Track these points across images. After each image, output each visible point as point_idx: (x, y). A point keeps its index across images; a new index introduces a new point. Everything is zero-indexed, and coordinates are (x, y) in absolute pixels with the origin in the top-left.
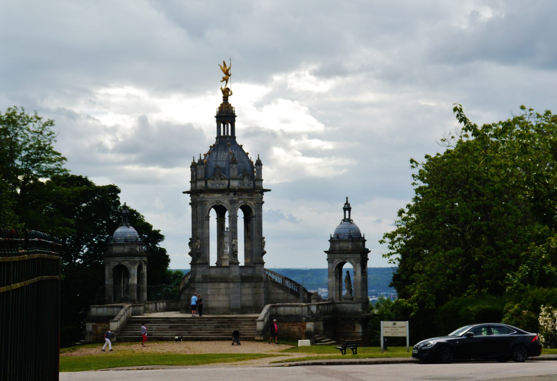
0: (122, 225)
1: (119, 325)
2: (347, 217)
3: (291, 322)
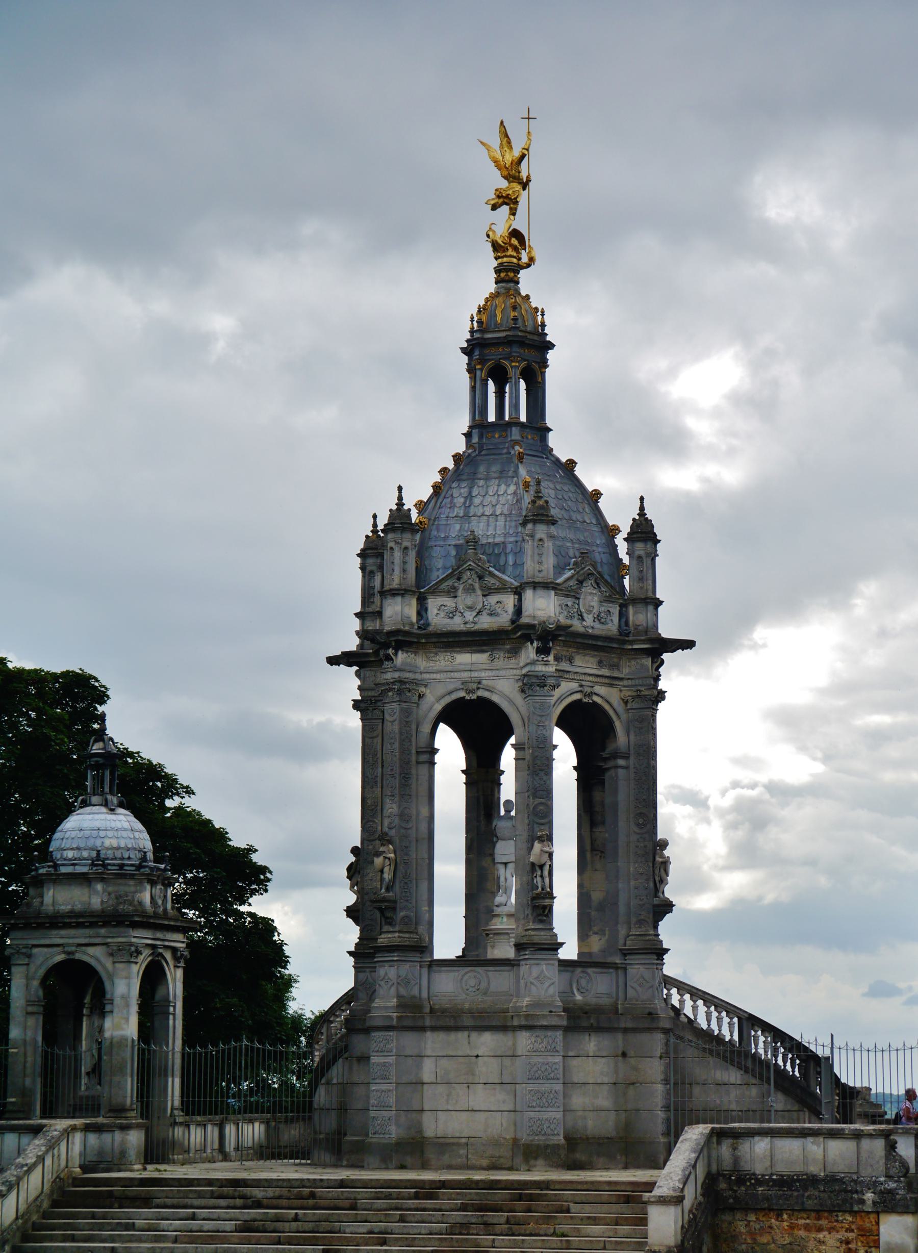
0: (85, 804)
3: (804, 1210)
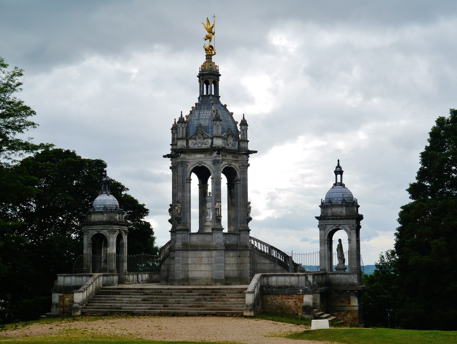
0: (102, 193)
1: (85, 297)
2: (339, 181)
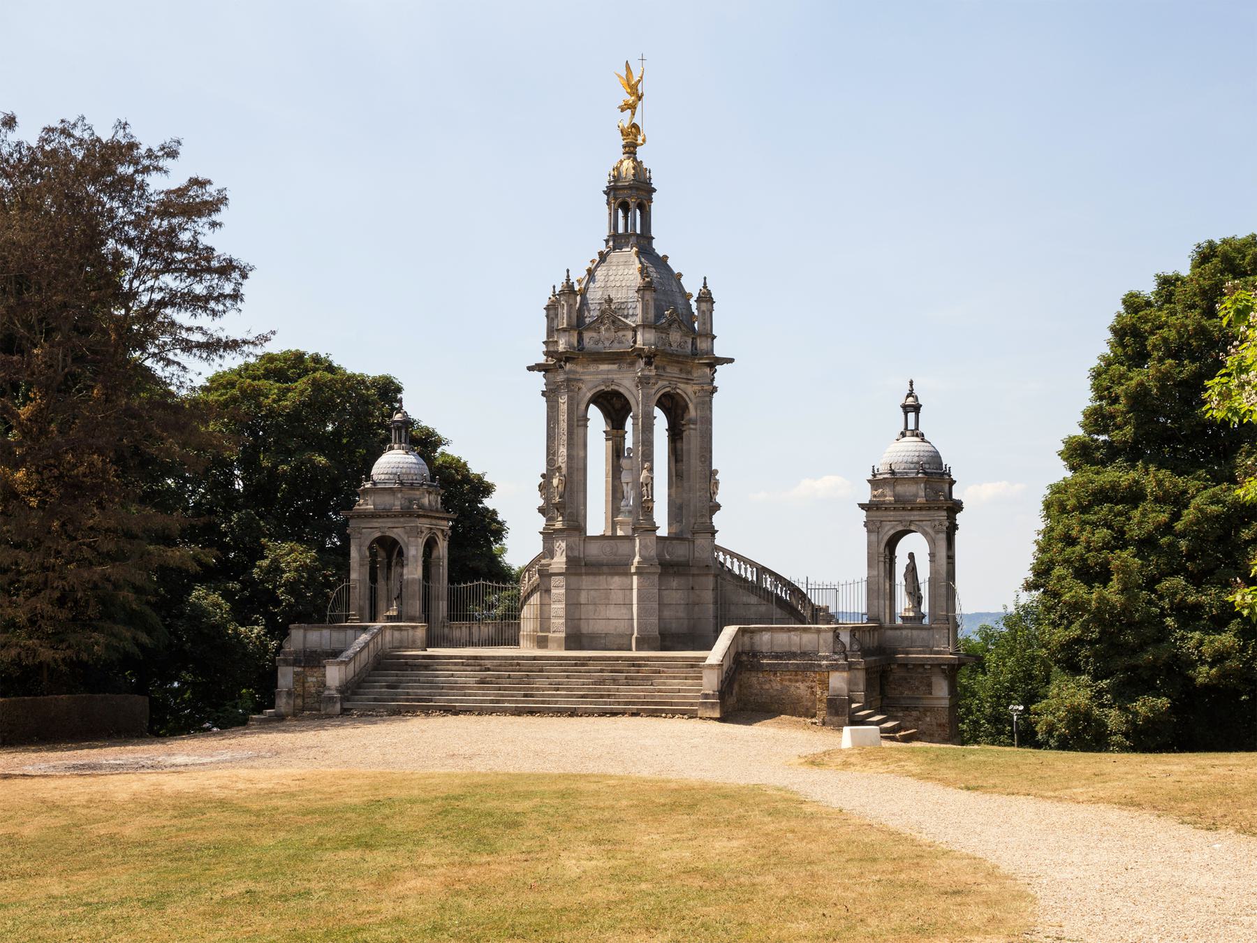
2: (911, 426)
